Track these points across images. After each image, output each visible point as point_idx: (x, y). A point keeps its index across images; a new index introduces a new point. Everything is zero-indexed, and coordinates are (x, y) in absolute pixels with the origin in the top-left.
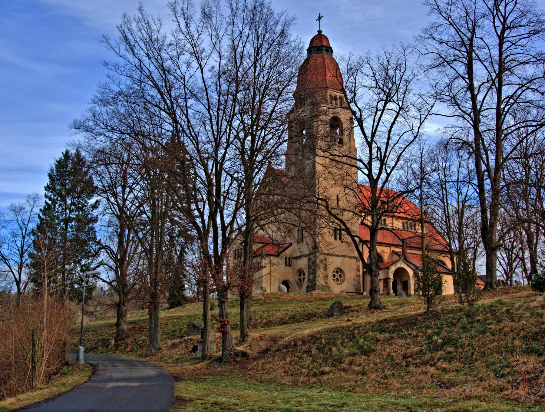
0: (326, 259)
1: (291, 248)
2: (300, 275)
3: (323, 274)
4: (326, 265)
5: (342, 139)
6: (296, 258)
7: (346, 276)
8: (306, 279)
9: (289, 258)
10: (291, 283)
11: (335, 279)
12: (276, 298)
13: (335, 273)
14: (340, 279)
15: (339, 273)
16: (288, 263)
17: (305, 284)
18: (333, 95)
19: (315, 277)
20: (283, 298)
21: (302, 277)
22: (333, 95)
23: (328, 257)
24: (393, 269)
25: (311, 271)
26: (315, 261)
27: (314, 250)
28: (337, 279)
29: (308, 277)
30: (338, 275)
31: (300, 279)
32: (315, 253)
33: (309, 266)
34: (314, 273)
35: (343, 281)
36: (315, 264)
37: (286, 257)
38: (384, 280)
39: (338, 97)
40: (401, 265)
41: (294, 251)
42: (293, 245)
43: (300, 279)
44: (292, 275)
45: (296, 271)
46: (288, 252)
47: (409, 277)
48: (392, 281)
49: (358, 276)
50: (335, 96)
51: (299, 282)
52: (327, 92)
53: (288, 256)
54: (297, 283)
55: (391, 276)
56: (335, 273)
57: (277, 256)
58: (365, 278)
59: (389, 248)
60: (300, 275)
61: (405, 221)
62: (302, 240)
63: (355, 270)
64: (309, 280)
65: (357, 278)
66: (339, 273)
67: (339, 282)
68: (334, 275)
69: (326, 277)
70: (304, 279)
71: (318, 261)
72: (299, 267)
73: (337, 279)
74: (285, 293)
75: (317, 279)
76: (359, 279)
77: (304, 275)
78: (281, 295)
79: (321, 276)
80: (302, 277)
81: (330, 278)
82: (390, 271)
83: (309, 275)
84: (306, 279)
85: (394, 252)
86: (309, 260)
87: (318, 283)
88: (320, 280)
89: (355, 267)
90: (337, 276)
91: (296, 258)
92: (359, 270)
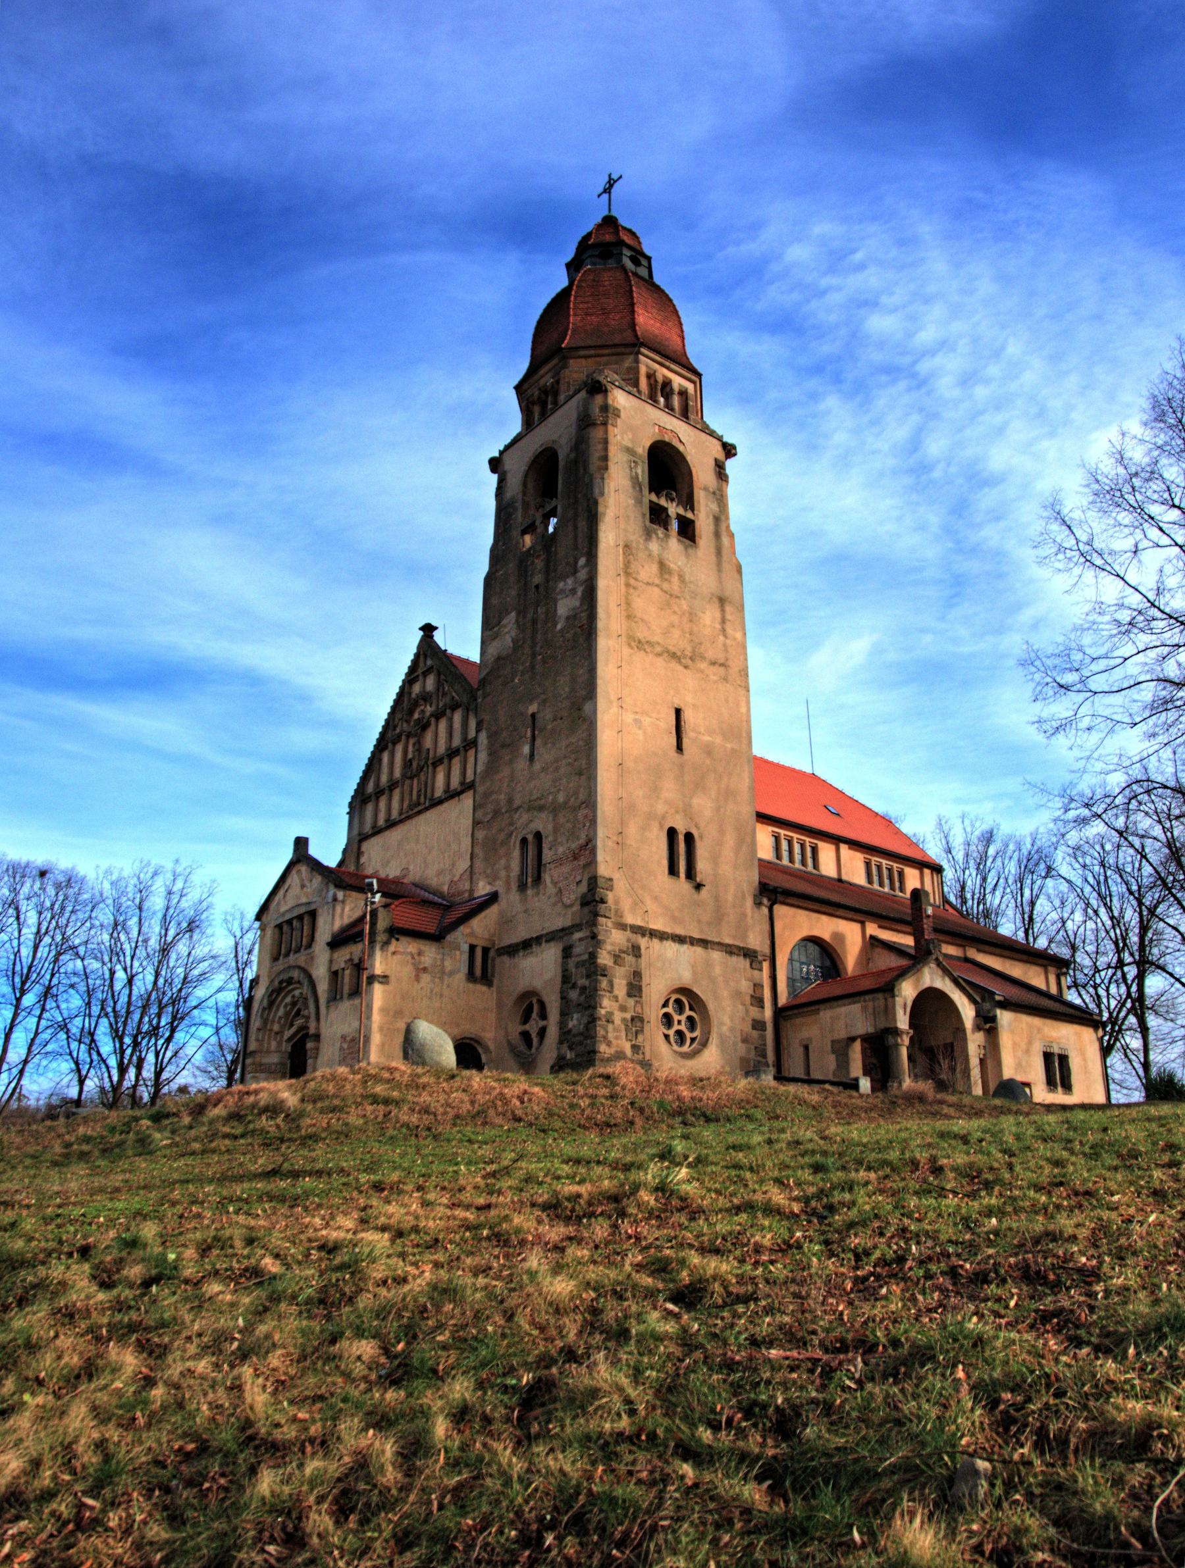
0: (636, 951)
1: (494, 910)
2: (526, 1018)
3: (623, 1009)
4: (637, 974)
5: (692, 522)
6: (512, 950)
7: (715, 1022)
8: (553, 1032)
9: (486, 951)
10: (487, 1050)
11: (671, 1032)
12: (375, 1100)
13: (670, 1009)
14: (689, 1035)
15: (688, 1012)
16: (478, 971)
17: (549, 1051)
18: (660, 379)
19: (593, 1020)
20: (425, 1098)
21: (533, 1027)
22: (660, 379)
23: (643, 942)
24: (908, 991)
25: (574, 995)
26: (593, 956)
27: (586, 909)
28: (679, 1033)
29: (562, 1024)
30: (683, 1018)
31: (526, 1035)
32: (594, 924)
33: (566, 978)
34: (589, 1004)
35: (704, 1044)
36: (593, 970)
37: (472, 948)
38: (866, 1039)
39: (676, 387)
40: (931, 977)
41: (506, 922)
42: (503, 902)
43: (526, 1035)
44: (492, 1017)
45: (509, 1002)
46: (481, 927)
47: (960, 1029)
48: (906, 1040)
49: (758, 1025)
50: (667, 384)
51: (522, 1047)
52: (637, 361)
53: (481, 943)
54: (513, 1049)
55: (903, 1022)
56: (670, 1009)
57: (437, 937)
58: (783, 1034)
59: (856, 927)
60: (526, 1018)
61: (875, 860)
62: (538, 879)
63: (748, 1000)
64: (565, 1035)
65: (755, 1034)
66: (688, 1012)
67: (686, 1048)
68: (668, 1020)
69: (637, 1022)
70: (542, 1032)
71: (604, 959)
72: (523, 984)
73: (679, 1033)
74: (439, 1072)
75: (600, 1032)
76: (763, 1038)
77: (543, 1015)
78: (414, 1084)
79: (618, 1017)
80: (533, 1027)
81: (655, 1032)
82: (899, 1001)
83: (564, 1014)
84: (553, 1032)
85: (874, 942)
86: (567, 952)
87: (602, 1048)
88: (611, 1036)
89: (745, 987)
90: (680, 1021)
91: (512, 950)
92: (759, 1002)
